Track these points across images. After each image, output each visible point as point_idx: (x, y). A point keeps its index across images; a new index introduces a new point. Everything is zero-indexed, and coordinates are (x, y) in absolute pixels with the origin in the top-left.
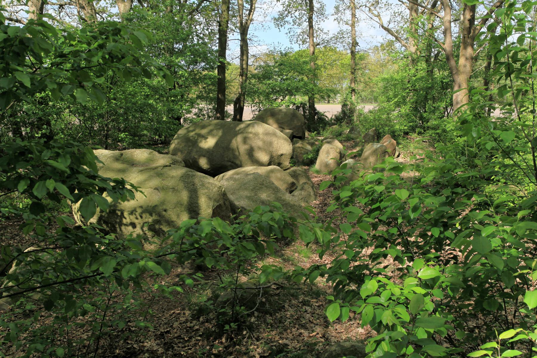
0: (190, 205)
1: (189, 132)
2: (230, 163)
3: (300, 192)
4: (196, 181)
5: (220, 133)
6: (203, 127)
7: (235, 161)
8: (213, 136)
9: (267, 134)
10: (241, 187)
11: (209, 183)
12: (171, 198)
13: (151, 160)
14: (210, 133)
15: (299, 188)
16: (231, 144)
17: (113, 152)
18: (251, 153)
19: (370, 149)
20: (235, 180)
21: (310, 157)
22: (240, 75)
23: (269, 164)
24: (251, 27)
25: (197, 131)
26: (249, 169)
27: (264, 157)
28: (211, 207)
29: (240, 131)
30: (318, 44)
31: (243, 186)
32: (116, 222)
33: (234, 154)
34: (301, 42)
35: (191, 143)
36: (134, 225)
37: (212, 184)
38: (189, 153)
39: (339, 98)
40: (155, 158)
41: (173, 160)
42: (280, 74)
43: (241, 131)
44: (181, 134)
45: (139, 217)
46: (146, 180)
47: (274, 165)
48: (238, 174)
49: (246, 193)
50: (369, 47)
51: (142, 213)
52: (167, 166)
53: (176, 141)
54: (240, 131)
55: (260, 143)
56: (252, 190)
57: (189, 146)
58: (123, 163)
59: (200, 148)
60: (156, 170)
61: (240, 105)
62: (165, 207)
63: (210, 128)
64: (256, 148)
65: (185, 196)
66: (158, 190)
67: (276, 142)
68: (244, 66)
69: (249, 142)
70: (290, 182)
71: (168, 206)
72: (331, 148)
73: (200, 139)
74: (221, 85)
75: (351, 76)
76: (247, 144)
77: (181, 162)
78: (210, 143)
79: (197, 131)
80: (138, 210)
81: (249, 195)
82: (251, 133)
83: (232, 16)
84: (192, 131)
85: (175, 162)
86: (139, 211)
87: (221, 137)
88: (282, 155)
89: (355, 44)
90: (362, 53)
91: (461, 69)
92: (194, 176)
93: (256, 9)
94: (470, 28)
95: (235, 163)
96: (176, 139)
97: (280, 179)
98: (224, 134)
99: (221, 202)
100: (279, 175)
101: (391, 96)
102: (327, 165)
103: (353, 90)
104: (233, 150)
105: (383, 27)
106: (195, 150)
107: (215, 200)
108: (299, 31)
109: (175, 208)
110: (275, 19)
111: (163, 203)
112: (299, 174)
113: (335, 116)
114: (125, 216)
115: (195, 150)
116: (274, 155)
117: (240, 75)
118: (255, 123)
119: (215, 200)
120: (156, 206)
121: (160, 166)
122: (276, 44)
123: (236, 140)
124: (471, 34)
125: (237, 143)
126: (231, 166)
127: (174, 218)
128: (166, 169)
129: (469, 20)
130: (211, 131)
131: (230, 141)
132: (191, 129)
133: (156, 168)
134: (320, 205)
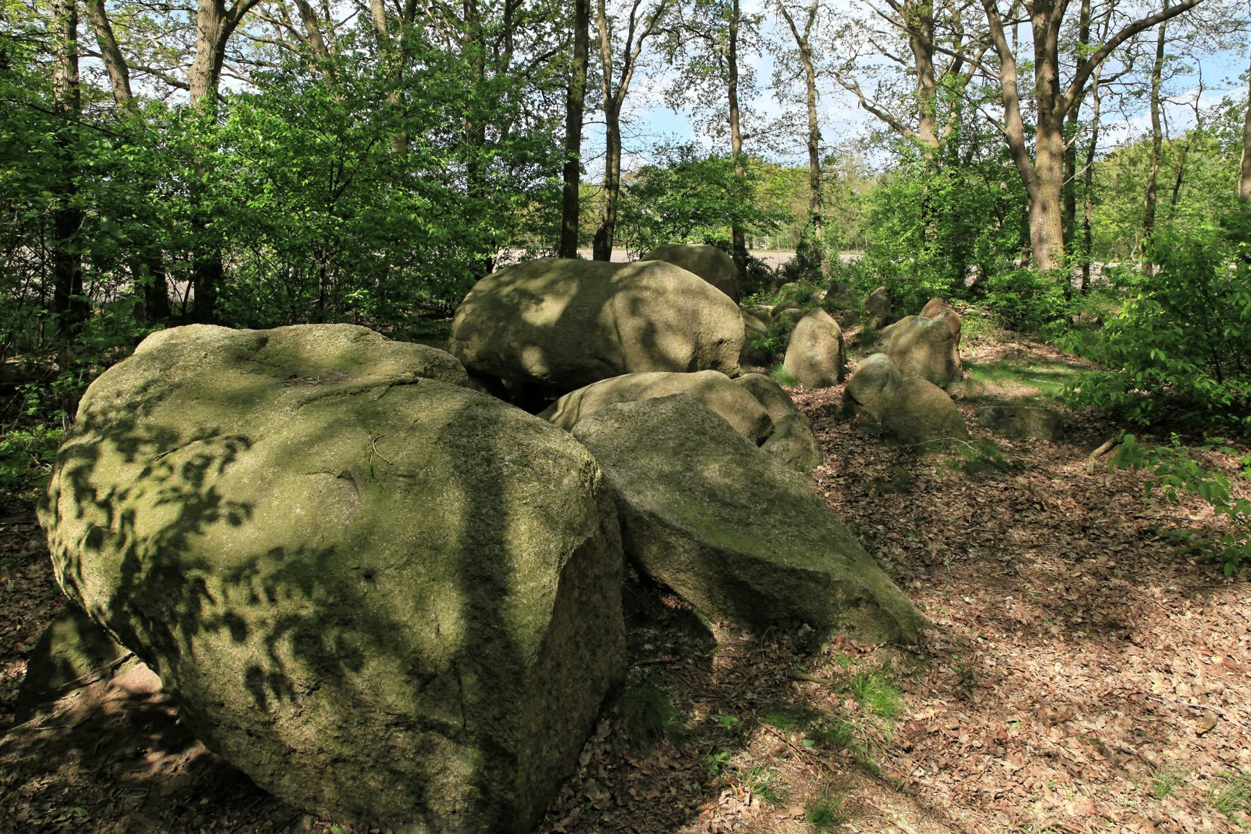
0: (471, 552)
1: (500, 285)
2: (596, 362)
3: (784, 442)
4: (501, 444)
5: (574, 288)
6: (534, 274)
7: (608, 357)
8: (558, 295)
9: (686, 292)
10: (639, 441)
11: (546, 453)
12: (400, 519)
13: (356, 361)
14: (550, 288)
15: (779, 430)
16: (602, 315)
17: (231, 331)
18: (648, 336)
19: (908, 331)
20: (622, 417)
21: (766, 344)
22: (606, 187)
23: (692, 367)
24: (625, 102)
25: (519, 284)
26: (649, 378)
27: (680, 350)
28: (554, 559)
29: (620, 285)
30: (747, 137)
31: (646, 438)
32: (174, 617)
33: (607, 341)
34: (715, 133)
35: (505, 311)
36: (239, 630)
37: (557, 456)
38: (499, 335)
39: (786, 232)
40: (369, 354)
41: (426, 359)
42: (678, 186)
43: (625, 282)
44: (481, 291)
45: (263, 596)
46: (316, 439)
47: (703, 369)
48: (623, 395)
49: (658, 463)
50: (841, 140)
51: (276, 577)
52: (402, 383)
53: (469, 308)
54: (620, 285)
55: (670, 315)
56: (676, 453)
57: (500, 320)
58: (259, 371)
59: (525, 323)
60: (360, 400)
61: (605, 243)
62: (367, 560)
63: (550, 276)
64: (659, 325)
65: (452, 508)
66: (351, 479)
67: (706, 311)
68: (614, 171)
69: (646, 310)
70: (757, 416)
71: (384, 556)
72: (819, 327)
73: (525, 302)
74: (570, 203)
75: (811, 194)
76: (640, 315)
77: (454, 367)
78: (549, 311)
79: (519, 284)
80: (261, 565)
81: (667, 469)
82: (647, 288)
83: (586, 76)
84: (508, 284)
85: (431, 370)
86: (266, 568)
87: (575, 298)
88: (721, 342)
89: (815, 135)
90: (829, 152)
91: (1045, 174)
92: (493, 421)
93: (637, 69)
94: (1053, 96)
95: (610, 363)
96: (468, 302)
97: (731, 408)
98: (583, 289)
99: (592, 532)
100: (728, 396)
101: (897, 228)
102: (813, 366)
103: (817, 218)
104: (604, 329)
105: (864, 105)
106: (512, 328)
107: (570, 528)
108: (711, 112)
109: (408, 563)
110: (667, 92)
111: (363, 540)
112: (766, 390)
113: (786, 266)
114: (212, 591)
115: (512, 328)
116: (704, 341)
117: (606, 187)
118: (657, 264)
119: (570, 528)
120: (331, 551)
121: (377, 385)
122: (669, 135)
123: (612, 305)
124: (1056, 108)
125: (614, 313)
126: (599, 368)
127: (403, 611)
128: (397, 397)
129: (1050, 82)
130: (553, 283)
131: (598, 309)
132: (505, 278)
133: (365, 389)
134: (841, 481)
